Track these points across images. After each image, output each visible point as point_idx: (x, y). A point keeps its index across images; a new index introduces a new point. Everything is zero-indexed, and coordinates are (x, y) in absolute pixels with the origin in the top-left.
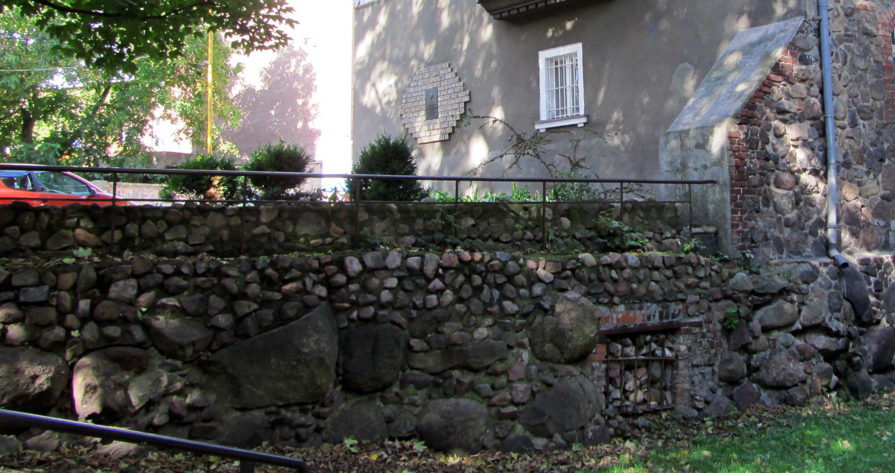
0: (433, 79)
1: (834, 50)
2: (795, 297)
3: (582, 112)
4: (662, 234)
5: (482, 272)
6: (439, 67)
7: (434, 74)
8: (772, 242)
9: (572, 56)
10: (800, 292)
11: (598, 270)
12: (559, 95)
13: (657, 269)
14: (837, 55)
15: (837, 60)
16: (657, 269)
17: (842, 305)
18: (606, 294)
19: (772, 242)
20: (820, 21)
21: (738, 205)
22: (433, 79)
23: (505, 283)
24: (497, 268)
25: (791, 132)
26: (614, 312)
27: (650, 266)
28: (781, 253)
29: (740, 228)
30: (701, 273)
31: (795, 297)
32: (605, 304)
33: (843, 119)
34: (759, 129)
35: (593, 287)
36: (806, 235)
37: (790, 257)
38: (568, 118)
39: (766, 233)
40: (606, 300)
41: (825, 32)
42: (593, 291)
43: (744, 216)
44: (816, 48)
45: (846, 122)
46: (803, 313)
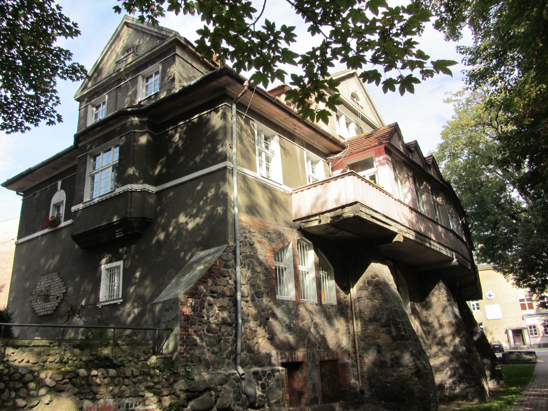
0: (49, 281)
1: (243, 262)
2: (213, 393)
3: (120, 296)
4: (138, 358)
5: (6, 381)
6: (53, 274)
7: (50, 278)
8: (203, 362)
9: (118, 267)
10: (216, 391)
11: (88, 379)
12: (111, 289)
13: (128, 377)
14: (244, 264)
15: (244, 267)
16: (128, 377)
17: (241, 397)
18: (91, 393)
19: (203, 362)
20: (236, 246)
21: (184, 342)
22: (49, 281)
23: (21, 387)
24: (17, 378)
25: (367, 361)
26: (96, 404)
27: (123, 376)
28: (209, 368)
29: (185, 354)
30: (156, 380)
31: (213, 393)
32: (91, 399)
33: (247, 297)
34: (199, 301)
35: (83, 389)
36: (224, 358)
37: (214, 371)
38: (114, 300)
39: (200, 357)
40: (91, 397)
41: (238, 252)
42: (83, 391)
43: (188, 348)
44: (233, 260)
45: (249, 299)
46: (218, 402)
